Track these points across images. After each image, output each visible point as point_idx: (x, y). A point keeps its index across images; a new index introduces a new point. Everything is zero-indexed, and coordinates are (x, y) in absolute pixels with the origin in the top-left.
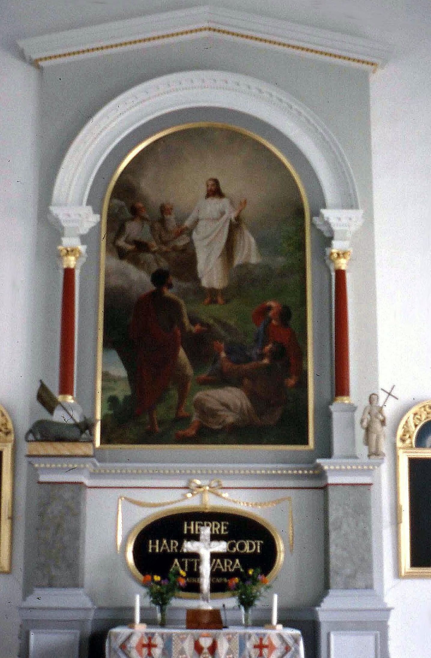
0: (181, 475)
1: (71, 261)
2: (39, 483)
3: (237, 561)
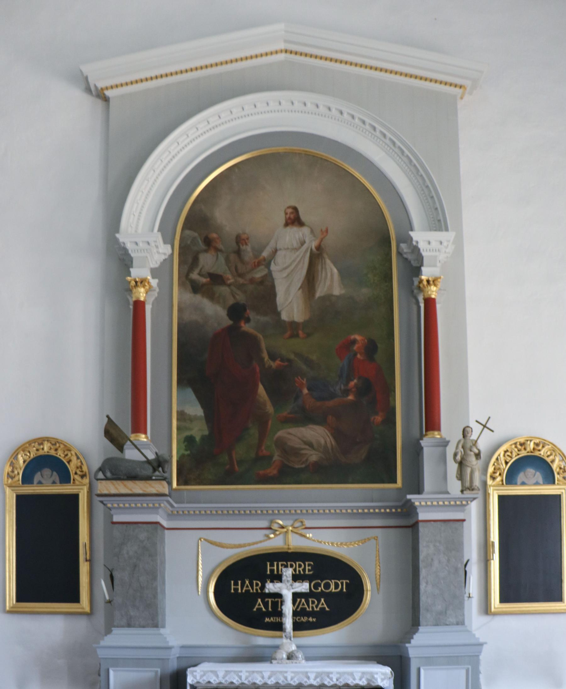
0: (263, 514)
1: (141, 294)
2: (113, 523)
3: (323, 600)
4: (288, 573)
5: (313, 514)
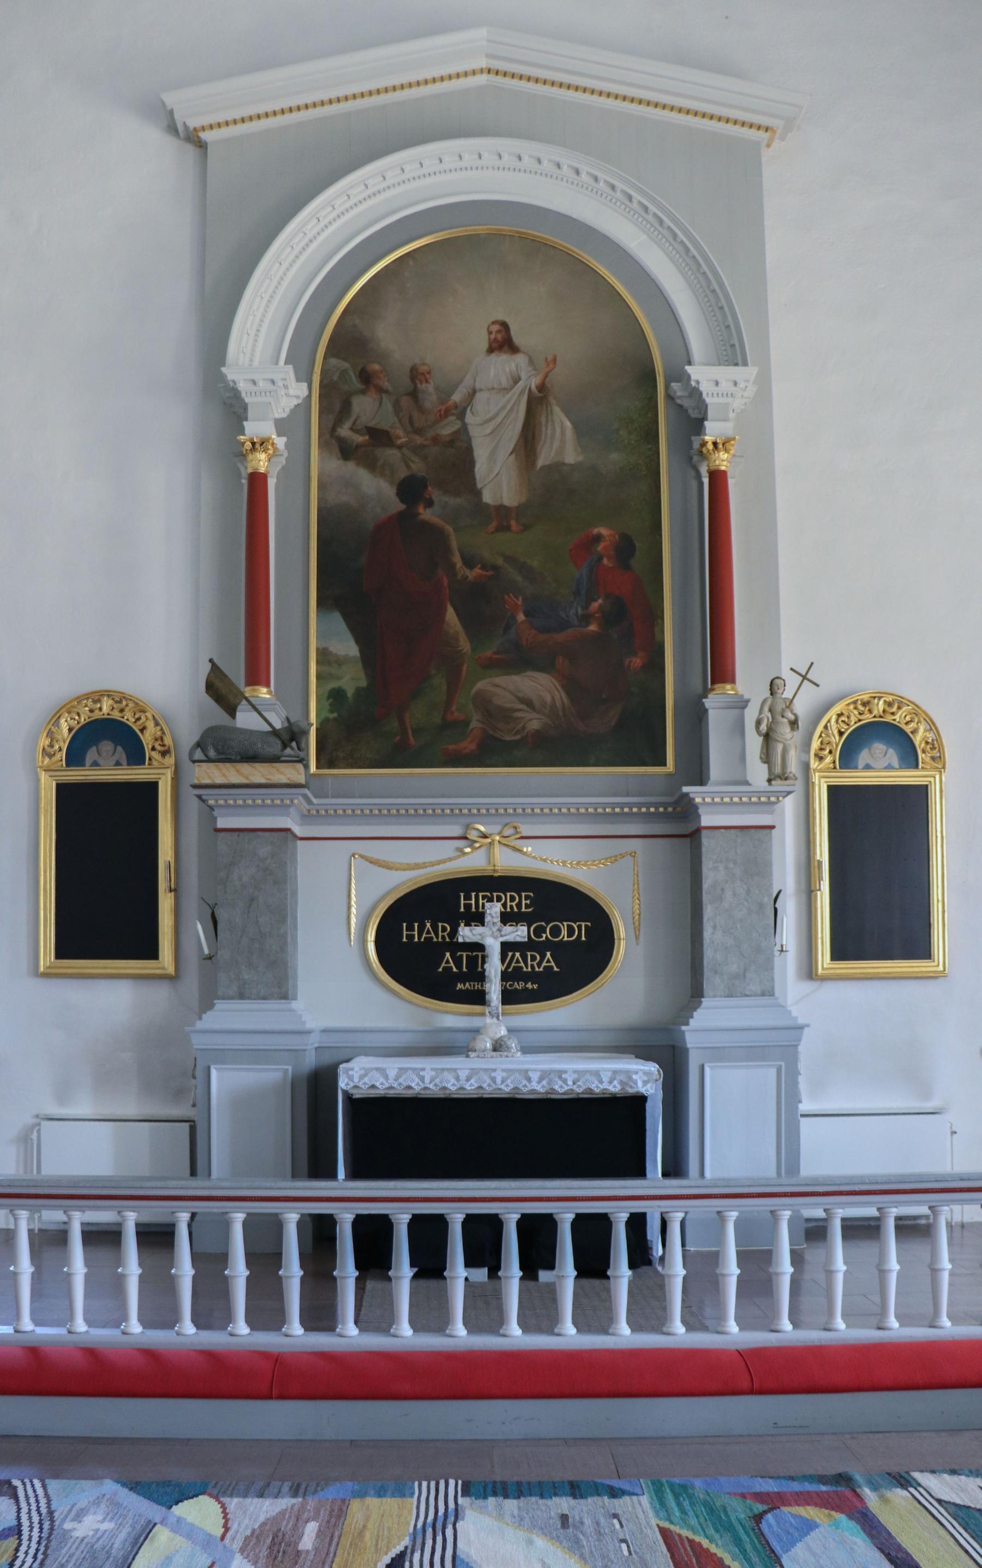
0: (454, 814)
1: (260, 462)
3: (548, 954)
4: (494, 910)
5: (533, 814)
